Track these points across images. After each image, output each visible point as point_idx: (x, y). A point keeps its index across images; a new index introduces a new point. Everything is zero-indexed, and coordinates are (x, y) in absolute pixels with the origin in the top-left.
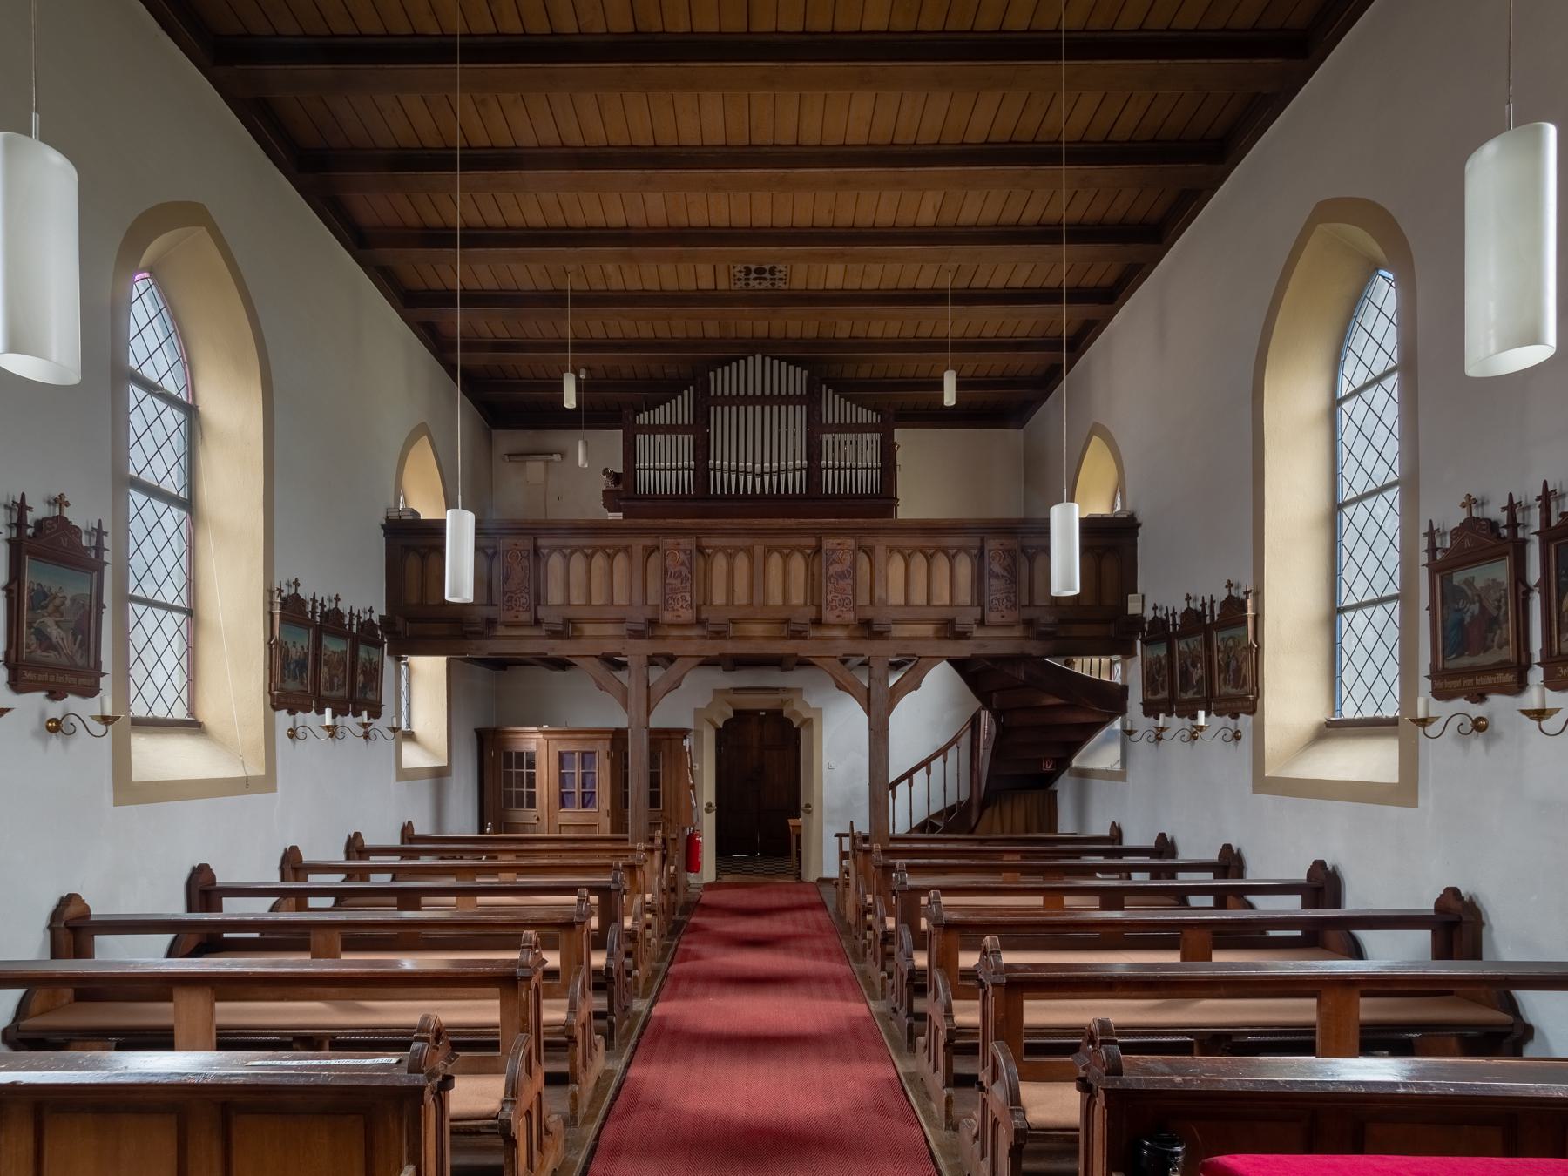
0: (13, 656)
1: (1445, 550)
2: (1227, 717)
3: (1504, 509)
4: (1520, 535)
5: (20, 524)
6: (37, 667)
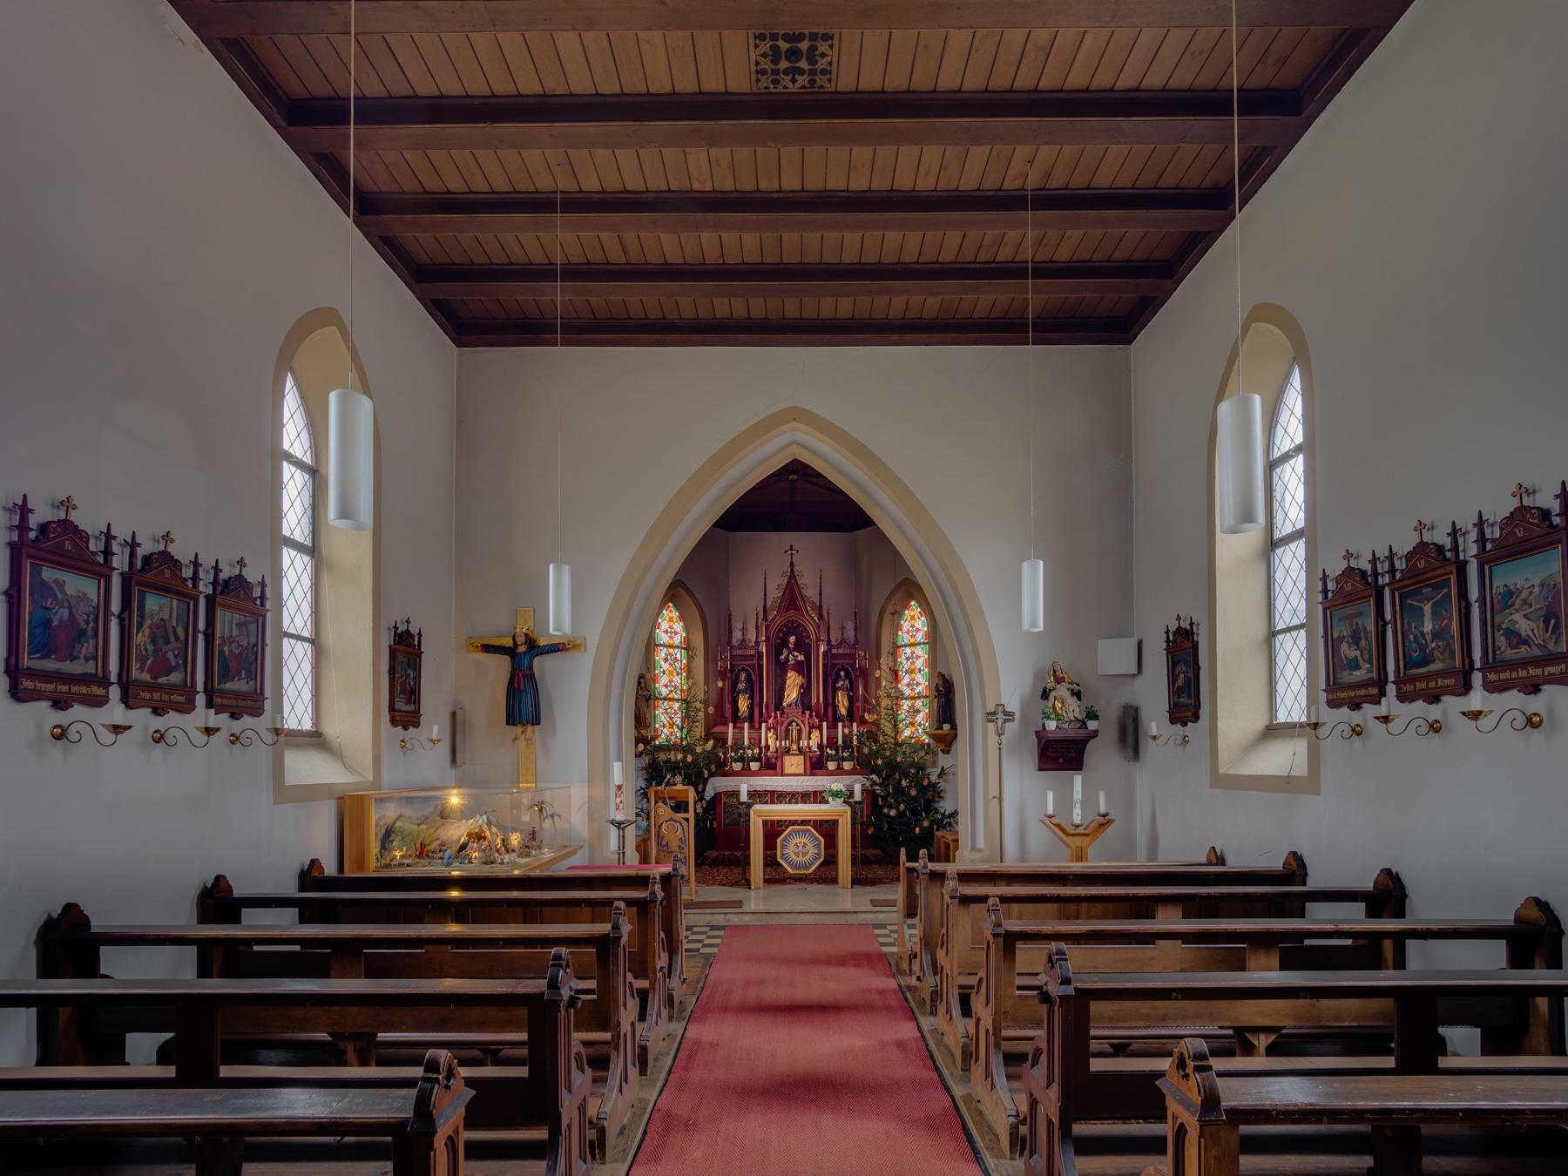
0: (13, 661)
1: (1493, 541)
2: (1345, 709)
3: (1557, 496)
4: (1462, 557)
5: (23, 527)
6: (223, 693)
